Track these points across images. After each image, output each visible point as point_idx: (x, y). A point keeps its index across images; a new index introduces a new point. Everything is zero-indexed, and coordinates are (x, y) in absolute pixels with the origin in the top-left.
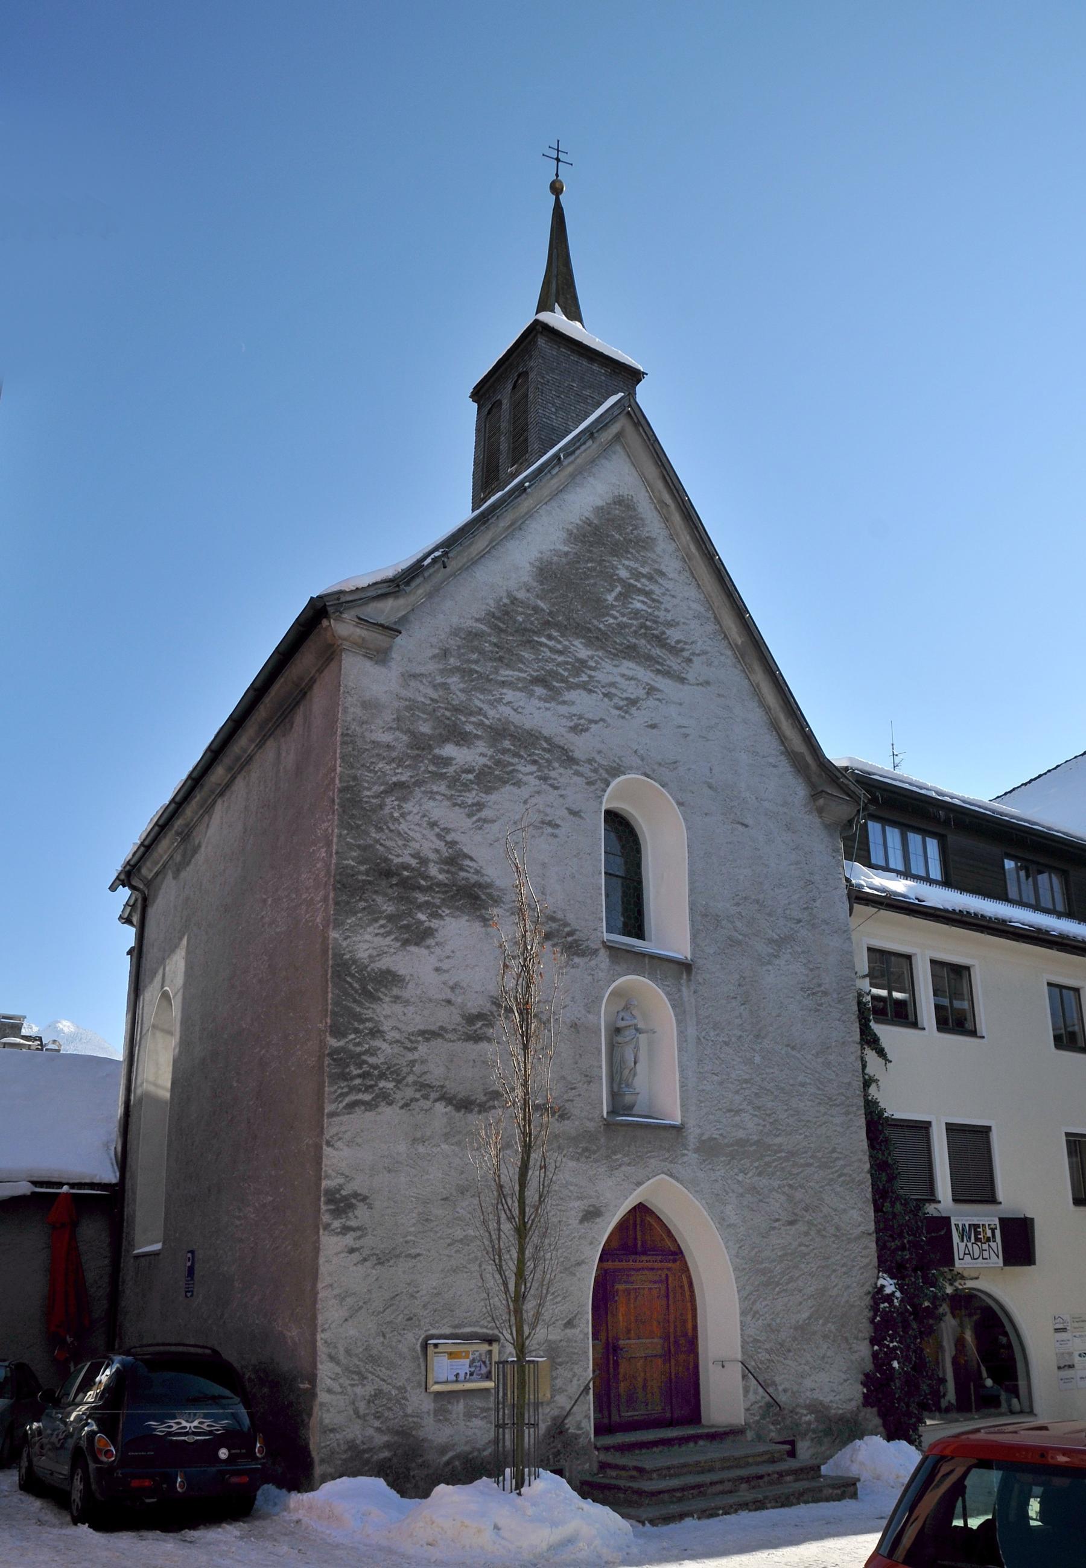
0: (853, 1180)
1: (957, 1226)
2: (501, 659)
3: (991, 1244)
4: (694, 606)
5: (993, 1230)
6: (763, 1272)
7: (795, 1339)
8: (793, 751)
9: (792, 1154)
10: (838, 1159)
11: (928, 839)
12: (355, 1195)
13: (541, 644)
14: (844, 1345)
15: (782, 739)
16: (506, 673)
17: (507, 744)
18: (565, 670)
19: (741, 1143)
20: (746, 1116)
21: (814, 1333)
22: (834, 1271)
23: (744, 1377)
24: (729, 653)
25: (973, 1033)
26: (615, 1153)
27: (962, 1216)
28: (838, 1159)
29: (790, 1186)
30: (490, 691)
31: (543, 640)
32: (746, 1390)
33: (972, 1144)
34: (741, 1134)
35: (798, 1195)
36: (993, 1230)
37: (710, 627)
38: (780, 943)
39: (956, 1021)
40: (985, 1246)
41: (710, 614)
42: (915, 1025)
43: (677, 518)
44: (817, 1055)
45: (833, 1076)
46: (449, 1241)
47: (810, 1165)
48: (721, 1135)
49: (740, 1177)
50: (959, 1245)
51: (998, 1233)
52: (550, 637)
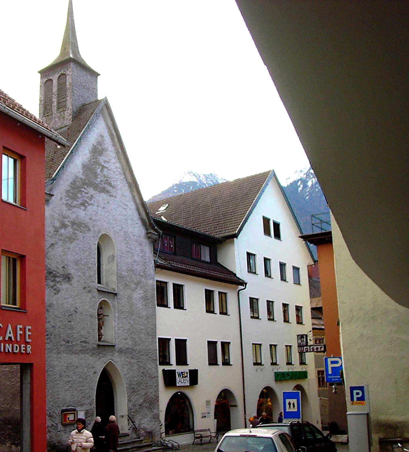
0: (153, 359)
1: (177, 372)
2: (73, 199)
3: (187, 378)
4: (119, 170)
5: (187, 373)
6: (132, 388)
7: (139, 408)
8: (143, 219)
9: (139, 352)
10: (150, 353)
11: (10, 158)
12: (84, 403)
13: (82, 191)
14: (151, 410)
15: (140, 214)
16: (75, 203)
17: (75, 227)
18: (88, 199)
19: (127, 349)
20: (128, 341)
21: (144, 407)
22: (149, 388)
23: (128, 420)
24: (127, 185)
25: (182, 308)
26: (100, 354)
27: (180, 369)
28: (150, 353)
29: (138, 362)
30: (71, 210)
31: (83, 190)
32: (129, 424)
33: (181, 344)
34: (128, 346)
35: (140, 364)
36: (187, 373)
37: (123, 177)
38: (137, 284)
39: (179, 305)
40: (185, 379)
41: (122, 172)
42: (166, 306)
43: (116, 139)
44: (145, 320)
45: (149, 326)
46: (65, 382)
47: (143, 355)
48: (123, 347)
49: (127, 360)
50: (178, 378)
51: (188, 374)
52: (85, 188)
